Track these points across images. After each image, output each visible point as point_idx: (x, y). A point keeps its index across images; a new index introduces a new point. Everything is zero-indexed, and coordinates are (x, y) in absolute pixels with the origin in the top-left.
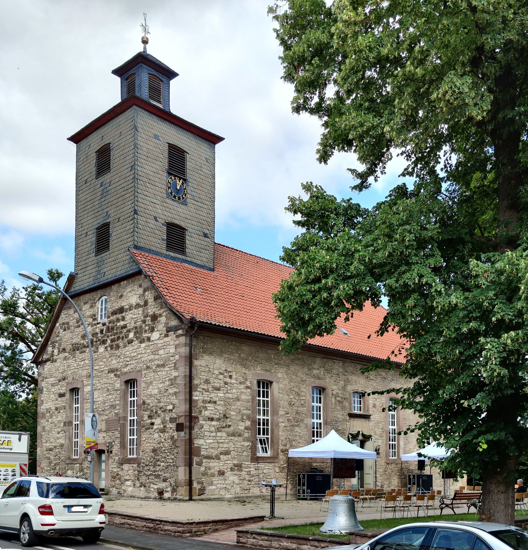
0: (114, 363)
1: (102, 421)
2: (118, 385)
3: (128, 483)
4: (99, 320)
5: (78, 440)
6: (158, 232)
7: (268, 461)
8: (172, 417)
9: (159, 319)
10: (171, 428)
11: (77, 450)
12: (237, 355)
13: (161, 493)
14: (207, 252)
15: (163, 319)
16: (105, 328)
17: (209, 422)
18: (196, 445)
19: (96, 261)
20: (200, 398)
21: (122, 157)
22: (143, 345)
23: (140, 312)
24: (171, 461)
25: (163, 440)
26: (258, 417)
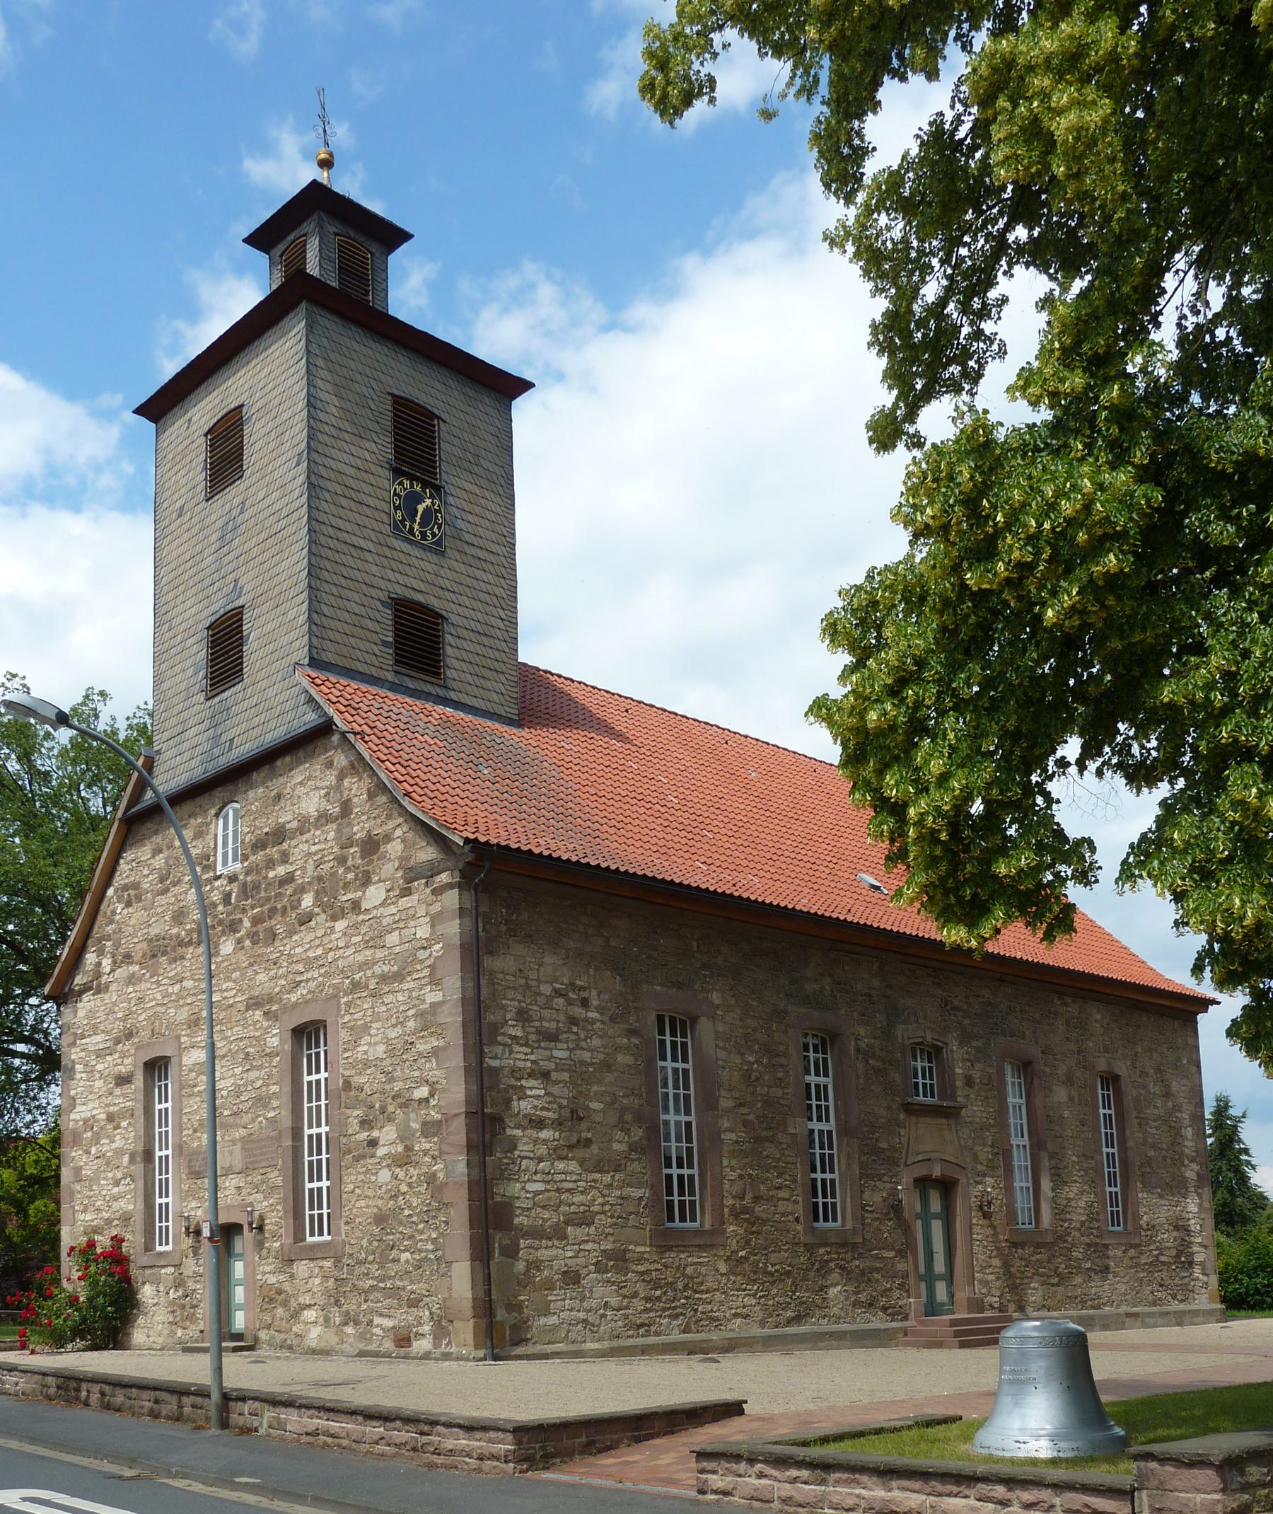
0: (262, 979)
1: (234, 1142)
2: (273, 1042)
3: (310, 1315)
4: (220, 869)
5: (169, 1200)
6: (370, 625)
7: (697, 1241)
8: (429, 1119)
9: (382, 849)
10: (426, 1152)
11: (167, 1227)
12: (601, 942)
13: (404, 1340)
14: (501, 676)
15: (394, 848)
16: (235, 887)
17: (532, 1132)
18: (498, 1199)
19: (208, 713)
20: (505, 1062)
21: (273, 435)
22: (340, 925)
23: (331, 835)
24: (430, 1247)
25: (404, 1188)
26: (663, 1117)
